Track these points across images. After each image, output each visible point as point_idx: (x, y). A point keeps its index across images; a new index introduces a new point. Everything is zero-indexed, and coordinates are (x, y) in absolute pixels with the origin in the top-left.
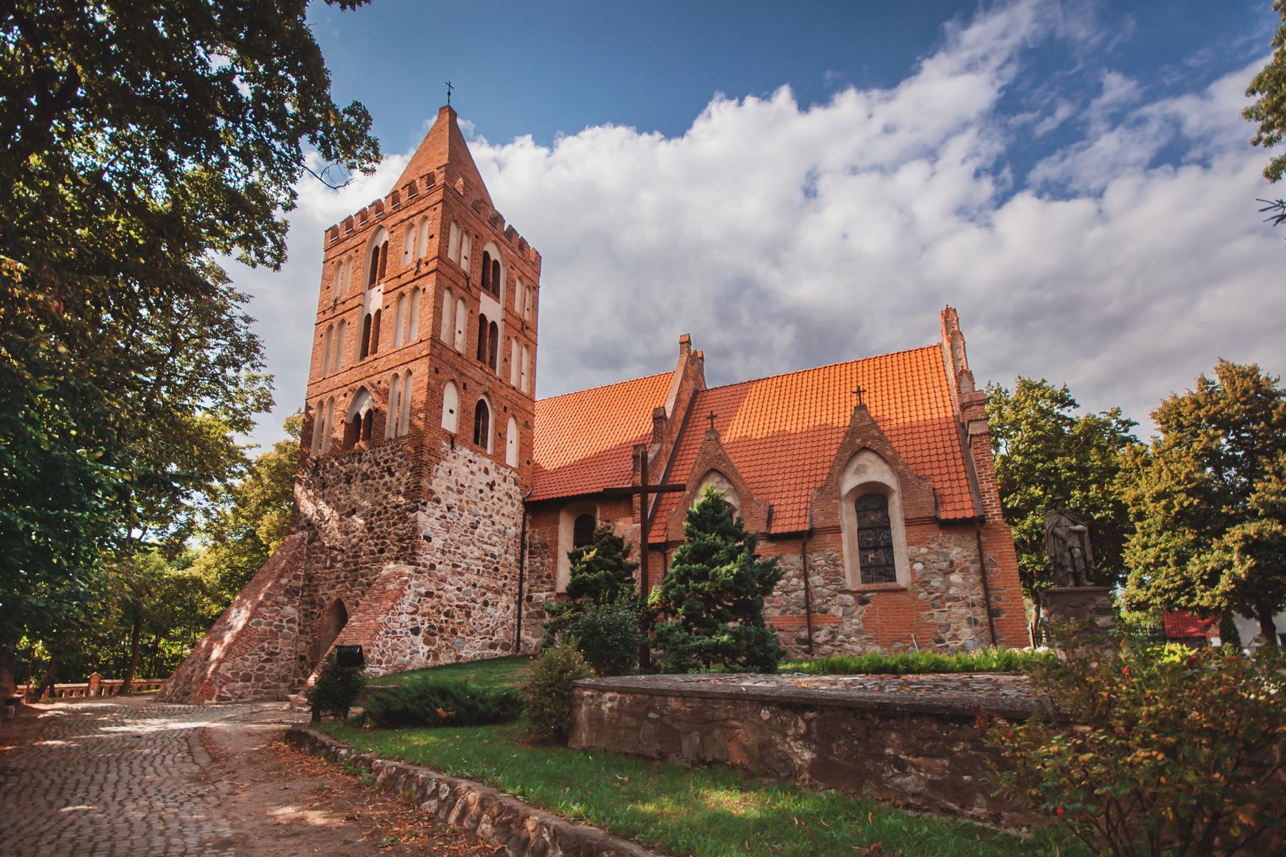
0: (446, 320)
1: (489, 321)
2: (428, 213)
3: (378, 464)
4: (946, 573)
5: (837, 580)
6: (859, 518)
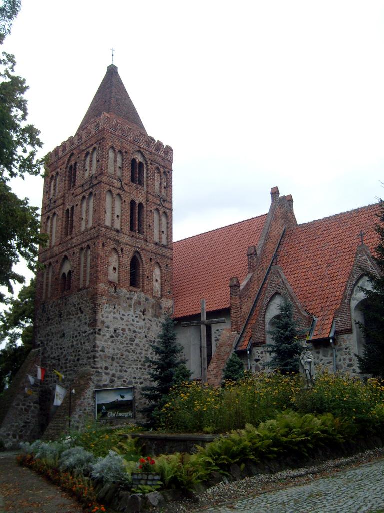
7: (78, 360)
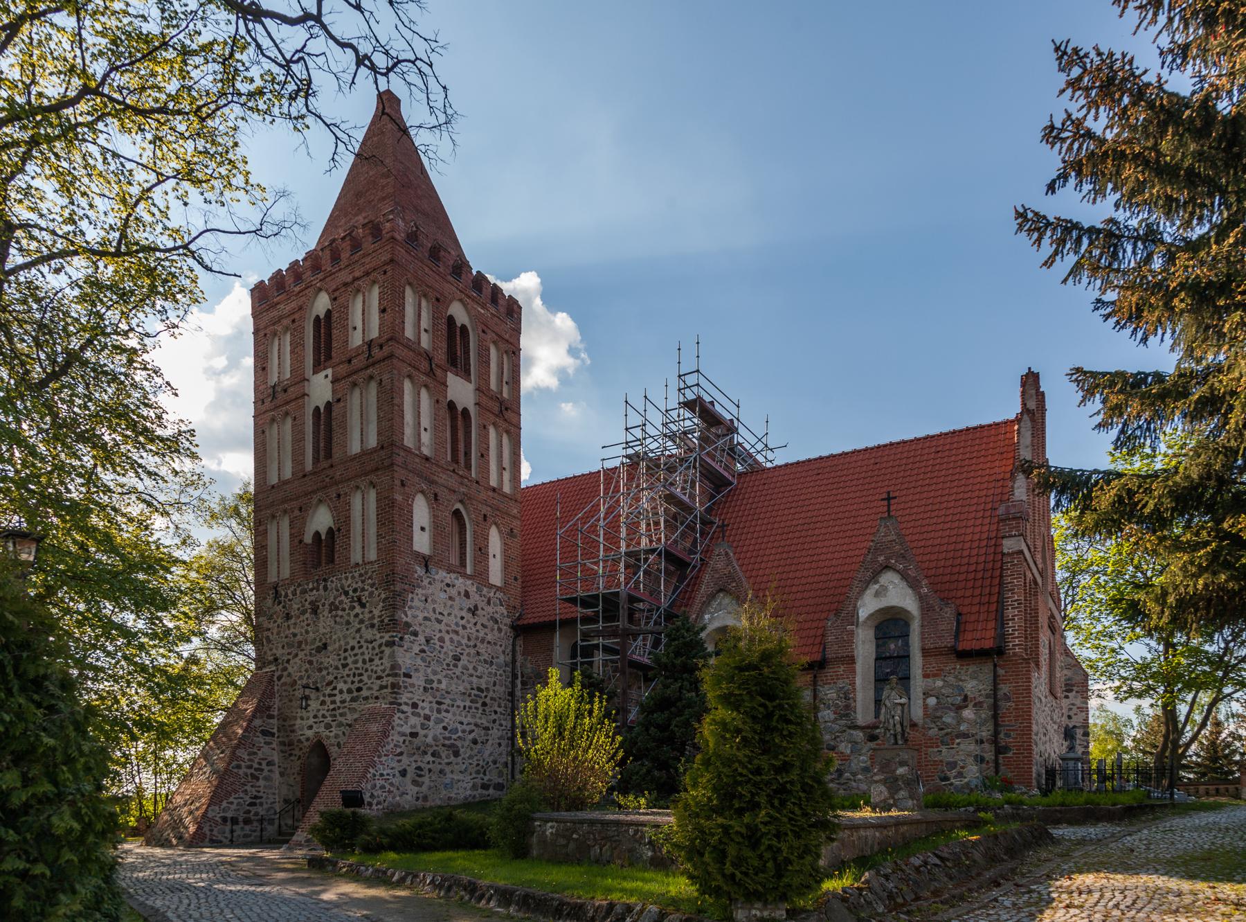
1: (460, 409)
3: (346, 593)
4: (959, 708)
5: (847, 715)
6: (878, 646)
7: (359, 689)
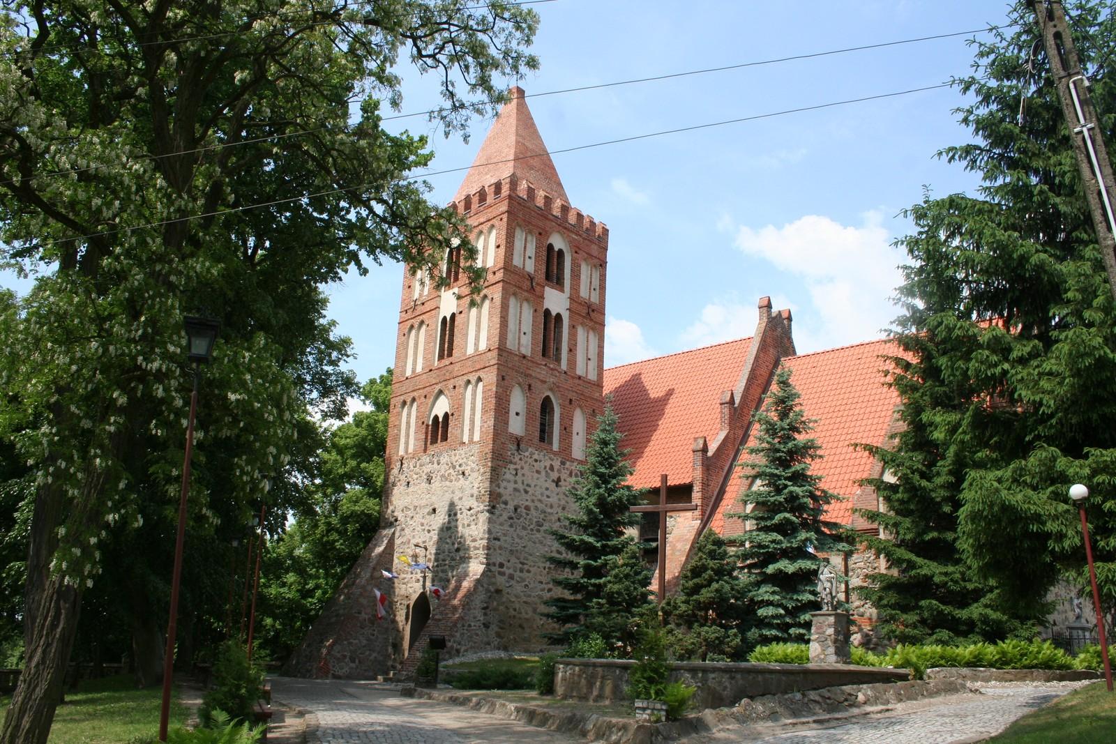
0: (512, 325)
2: (495, 222)
3: (454, 467)
